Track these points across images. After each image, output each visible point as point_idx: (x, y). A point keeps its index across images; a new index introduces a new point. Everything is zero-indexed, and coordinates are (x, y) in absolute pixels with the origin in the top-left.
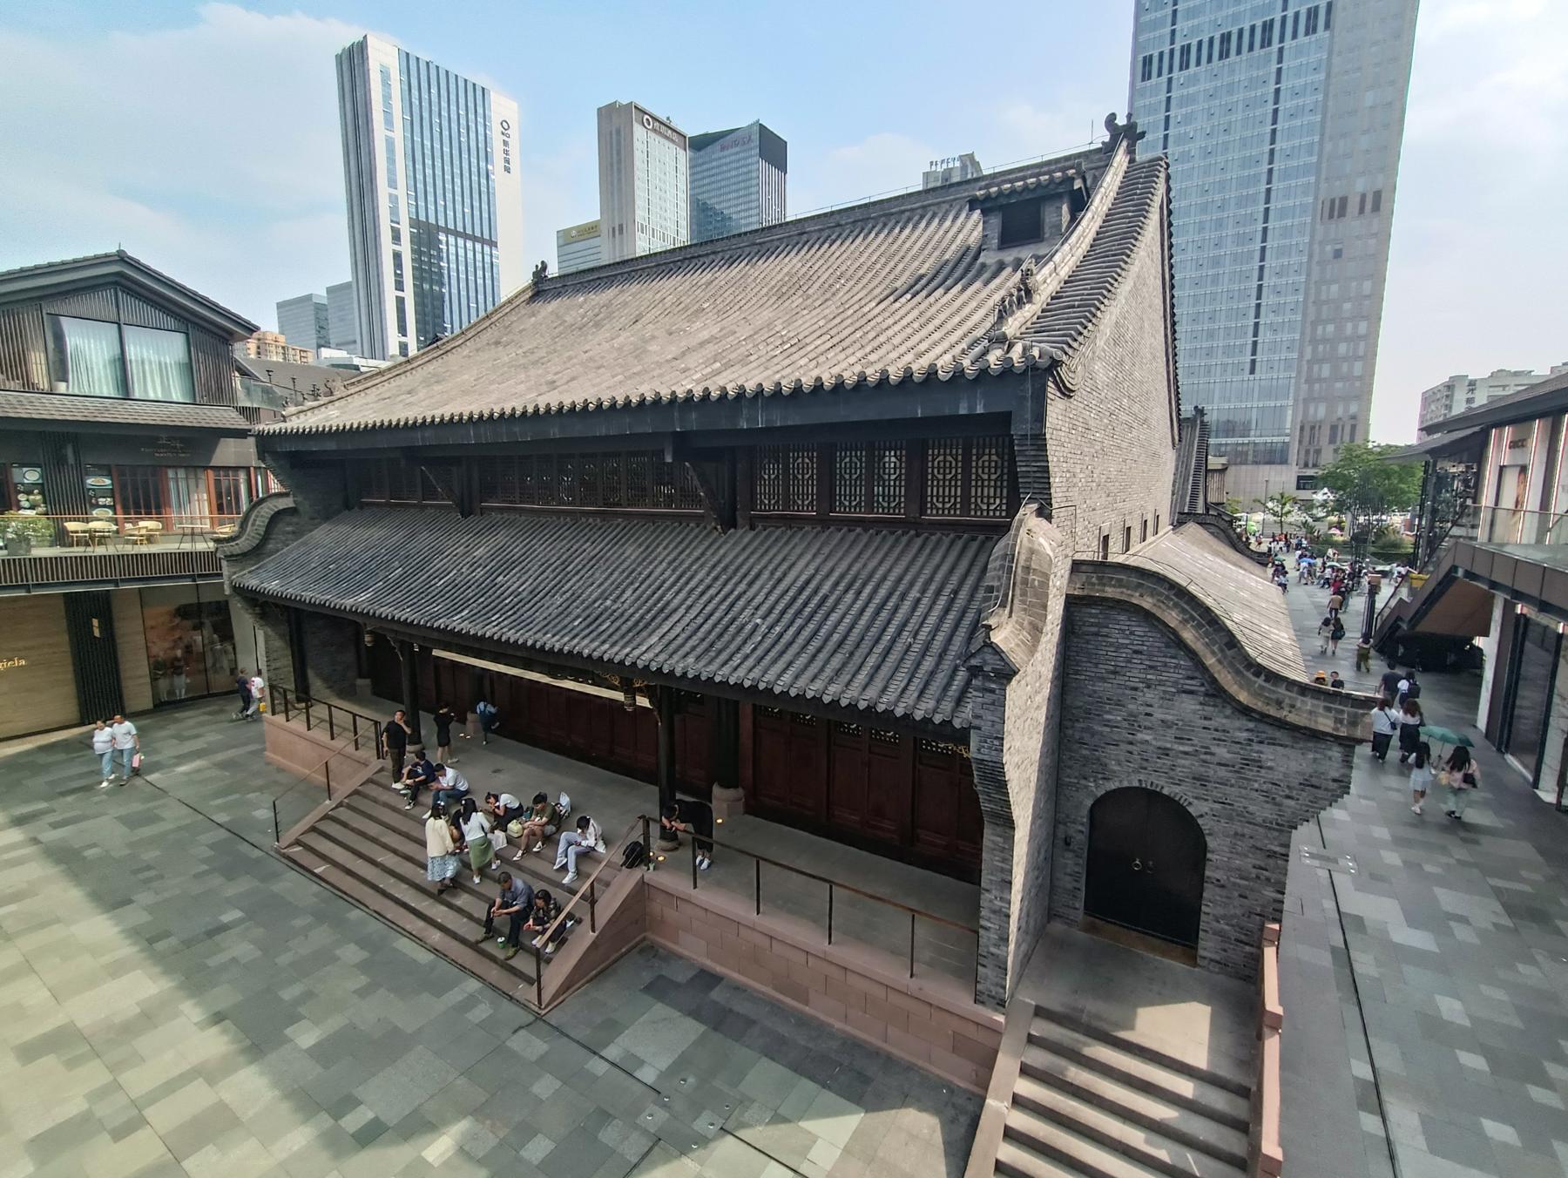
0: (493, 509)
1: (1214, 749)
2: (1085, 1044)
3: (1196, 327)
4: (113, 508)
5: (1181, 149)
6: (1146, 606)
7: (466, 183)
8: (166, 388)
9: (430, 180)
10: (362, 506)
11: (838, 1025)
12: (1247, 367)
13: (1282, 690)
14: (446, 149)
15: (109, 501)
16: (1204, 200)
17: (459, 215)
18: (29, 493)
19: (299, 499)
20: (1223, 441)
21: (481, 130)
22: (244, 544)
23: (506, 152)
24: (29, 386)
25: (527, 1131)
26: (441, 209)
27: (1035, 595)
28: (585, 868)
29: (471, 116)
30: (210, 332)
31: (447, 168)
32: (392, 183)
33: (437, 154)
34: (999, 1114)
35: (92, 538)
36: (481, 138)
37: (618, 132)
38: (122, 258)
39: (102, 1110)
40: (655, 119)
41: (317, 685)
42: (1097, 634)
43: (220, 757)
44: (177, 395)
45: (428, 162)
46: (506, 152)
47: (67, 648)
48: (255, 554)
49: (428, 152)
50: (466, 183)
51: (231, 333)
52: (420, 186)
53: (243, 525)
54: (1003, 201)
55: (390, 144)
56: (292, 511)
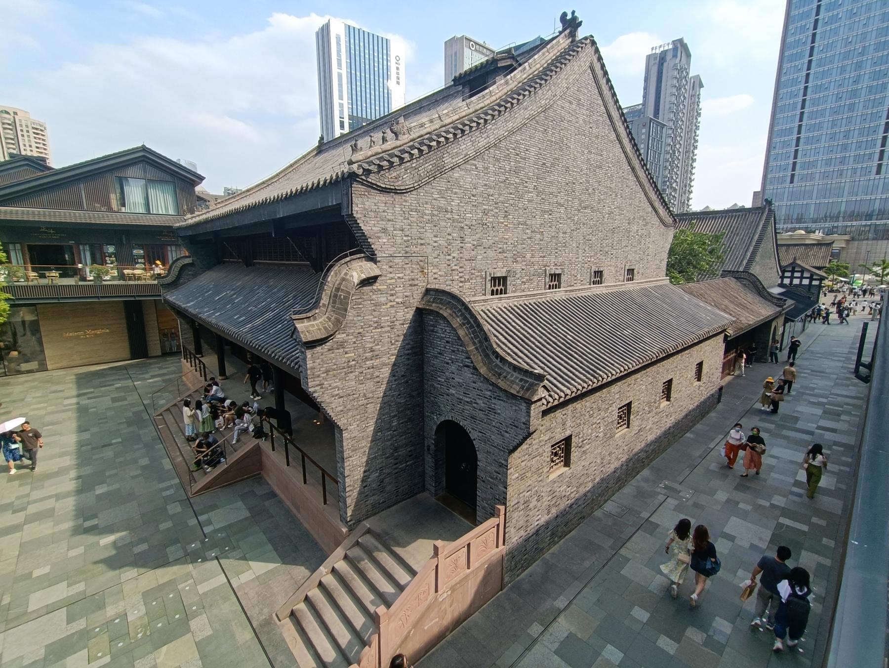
0: (260, 263)
1: (478, 401)
2: (379, 550)
3: (832, 143)
4: (144, 264)
5: (831, 14)
6: (445, 315)
7: (377, 93)
8: (167, 209)
9: (359, 93)
10: (224, 262)
11: (306, 525)
12: (874, 170)
13: (506, 368)
14: (367, 76)
15: (142, 261)
16: (847, 49)
17: (373, 111)
18: (110, 257)
19: (195, 259)
20: (849, 224)
21: (385, 62)
22: (169, 280)
23: (398, 74)
24: (110, 209)
25: (141, 541)
26: (364, 109)
27: (341, 303)
28: (243, 438)
29: (380, 56)
30: (182, 180)
31: (368, 86)
32: (341, 98)
33: (363, 79)
34: (321, 573)
35: (135, 277)
36: (385, 67)
37: (456, 54)
38: (144, 149)
39: (17, 503)
40: (476, 43)
41: (205, 347)
42: (433, 331)
43: (167, 377)
44: (171, 212)
45: (358, 84)
46: (398, 74)
47: (125, 325)
48: (174, 284)
49: (358, 78)
50: (377, 93)
51: (194, 181)
52: (354, 97)
53: (169, 270)
54: (468, 78)
55: (340, 76)
56: (192, 265)
